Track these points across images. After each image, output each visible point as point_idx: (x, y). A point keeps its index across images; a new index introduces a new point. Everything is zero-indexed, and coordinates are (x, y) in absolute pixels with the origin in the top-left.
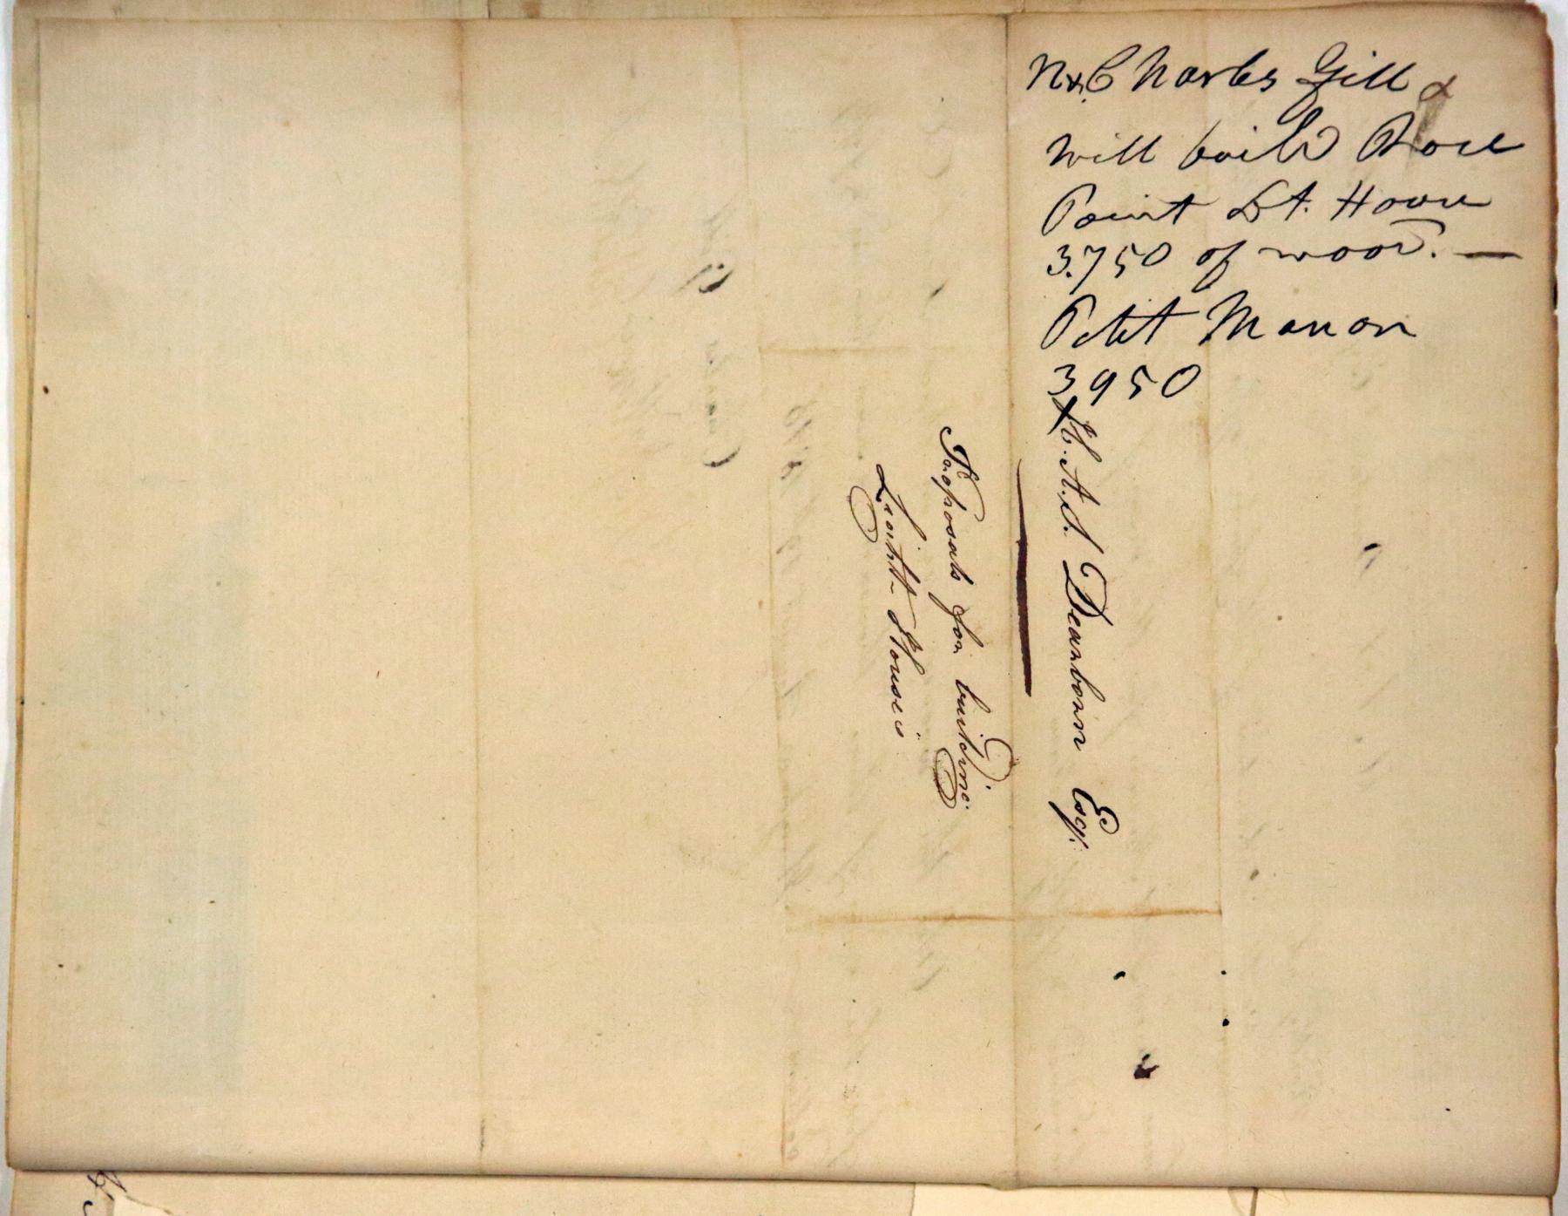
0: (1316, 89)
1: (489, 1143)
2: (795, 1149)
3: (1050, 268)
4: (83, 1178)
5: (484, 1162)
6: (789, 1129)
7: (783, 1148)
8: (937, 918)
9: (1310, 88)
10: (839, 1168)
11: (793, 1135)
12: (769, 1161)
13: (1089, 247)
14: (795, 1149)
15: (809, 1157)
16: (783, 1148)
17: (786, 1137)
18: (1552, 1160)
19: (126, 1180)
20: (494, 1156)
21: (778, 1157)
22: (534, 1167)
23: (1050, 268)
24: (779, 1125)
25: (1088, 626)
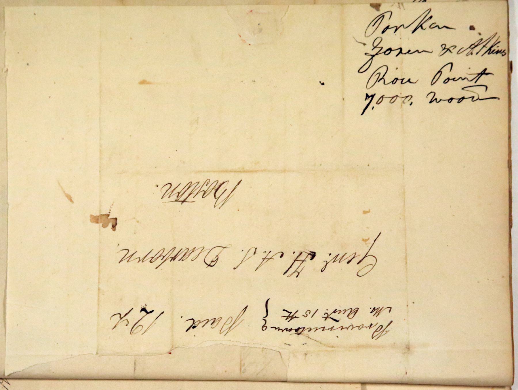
0: (372, 58)
1: (137, 368)
2: (245, 369)
3: (282, 256)
4: (296, 262)
5: (136, 375)
6: (242, 363)
7: (241, 370)
8: (269, 171)
9: (370, 57)
10: (261, 376)
11: (244, 364)
12: (236, 374)
13: (283, 254)
14: (245, 369)
15: (251, 371)
16: (241, 370)
17: (241, 365)
18: (512, 380)
19: (10, 381)
20: (139, 373)
21: (238, 372)
22: (154, 376)
23: (282, 256)
24: (239, 361)
25: (411, 81)
